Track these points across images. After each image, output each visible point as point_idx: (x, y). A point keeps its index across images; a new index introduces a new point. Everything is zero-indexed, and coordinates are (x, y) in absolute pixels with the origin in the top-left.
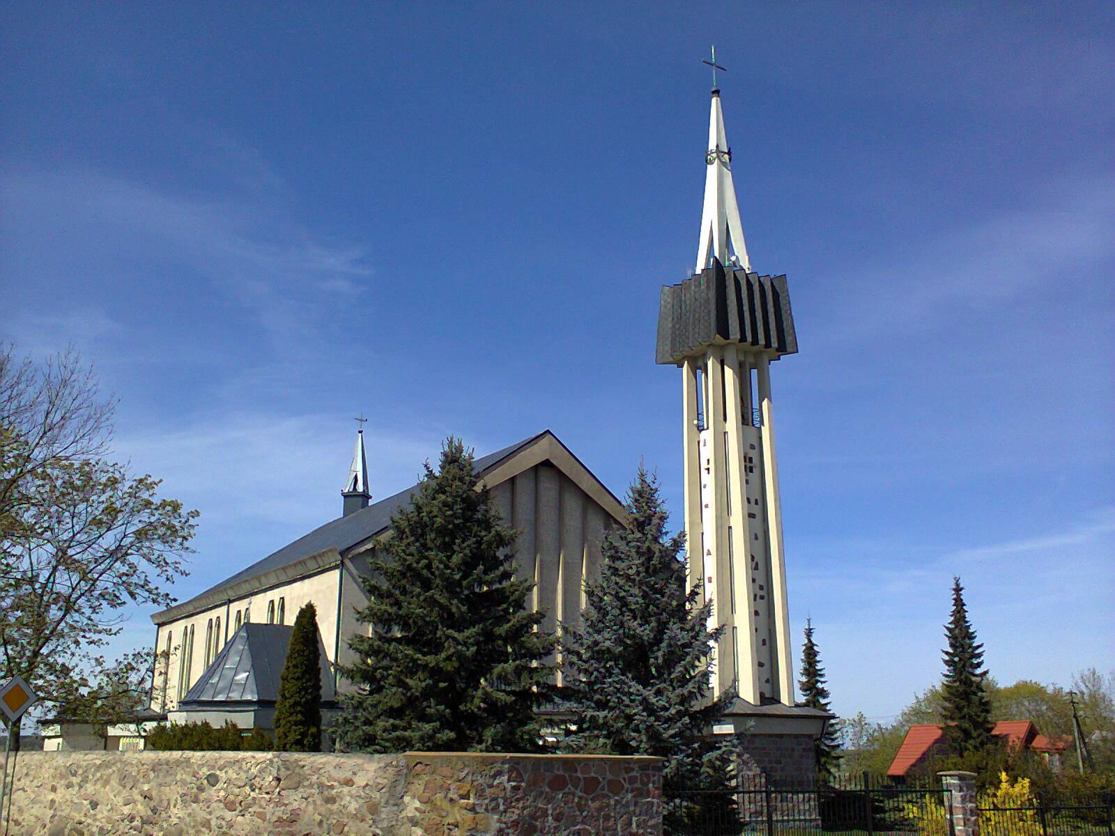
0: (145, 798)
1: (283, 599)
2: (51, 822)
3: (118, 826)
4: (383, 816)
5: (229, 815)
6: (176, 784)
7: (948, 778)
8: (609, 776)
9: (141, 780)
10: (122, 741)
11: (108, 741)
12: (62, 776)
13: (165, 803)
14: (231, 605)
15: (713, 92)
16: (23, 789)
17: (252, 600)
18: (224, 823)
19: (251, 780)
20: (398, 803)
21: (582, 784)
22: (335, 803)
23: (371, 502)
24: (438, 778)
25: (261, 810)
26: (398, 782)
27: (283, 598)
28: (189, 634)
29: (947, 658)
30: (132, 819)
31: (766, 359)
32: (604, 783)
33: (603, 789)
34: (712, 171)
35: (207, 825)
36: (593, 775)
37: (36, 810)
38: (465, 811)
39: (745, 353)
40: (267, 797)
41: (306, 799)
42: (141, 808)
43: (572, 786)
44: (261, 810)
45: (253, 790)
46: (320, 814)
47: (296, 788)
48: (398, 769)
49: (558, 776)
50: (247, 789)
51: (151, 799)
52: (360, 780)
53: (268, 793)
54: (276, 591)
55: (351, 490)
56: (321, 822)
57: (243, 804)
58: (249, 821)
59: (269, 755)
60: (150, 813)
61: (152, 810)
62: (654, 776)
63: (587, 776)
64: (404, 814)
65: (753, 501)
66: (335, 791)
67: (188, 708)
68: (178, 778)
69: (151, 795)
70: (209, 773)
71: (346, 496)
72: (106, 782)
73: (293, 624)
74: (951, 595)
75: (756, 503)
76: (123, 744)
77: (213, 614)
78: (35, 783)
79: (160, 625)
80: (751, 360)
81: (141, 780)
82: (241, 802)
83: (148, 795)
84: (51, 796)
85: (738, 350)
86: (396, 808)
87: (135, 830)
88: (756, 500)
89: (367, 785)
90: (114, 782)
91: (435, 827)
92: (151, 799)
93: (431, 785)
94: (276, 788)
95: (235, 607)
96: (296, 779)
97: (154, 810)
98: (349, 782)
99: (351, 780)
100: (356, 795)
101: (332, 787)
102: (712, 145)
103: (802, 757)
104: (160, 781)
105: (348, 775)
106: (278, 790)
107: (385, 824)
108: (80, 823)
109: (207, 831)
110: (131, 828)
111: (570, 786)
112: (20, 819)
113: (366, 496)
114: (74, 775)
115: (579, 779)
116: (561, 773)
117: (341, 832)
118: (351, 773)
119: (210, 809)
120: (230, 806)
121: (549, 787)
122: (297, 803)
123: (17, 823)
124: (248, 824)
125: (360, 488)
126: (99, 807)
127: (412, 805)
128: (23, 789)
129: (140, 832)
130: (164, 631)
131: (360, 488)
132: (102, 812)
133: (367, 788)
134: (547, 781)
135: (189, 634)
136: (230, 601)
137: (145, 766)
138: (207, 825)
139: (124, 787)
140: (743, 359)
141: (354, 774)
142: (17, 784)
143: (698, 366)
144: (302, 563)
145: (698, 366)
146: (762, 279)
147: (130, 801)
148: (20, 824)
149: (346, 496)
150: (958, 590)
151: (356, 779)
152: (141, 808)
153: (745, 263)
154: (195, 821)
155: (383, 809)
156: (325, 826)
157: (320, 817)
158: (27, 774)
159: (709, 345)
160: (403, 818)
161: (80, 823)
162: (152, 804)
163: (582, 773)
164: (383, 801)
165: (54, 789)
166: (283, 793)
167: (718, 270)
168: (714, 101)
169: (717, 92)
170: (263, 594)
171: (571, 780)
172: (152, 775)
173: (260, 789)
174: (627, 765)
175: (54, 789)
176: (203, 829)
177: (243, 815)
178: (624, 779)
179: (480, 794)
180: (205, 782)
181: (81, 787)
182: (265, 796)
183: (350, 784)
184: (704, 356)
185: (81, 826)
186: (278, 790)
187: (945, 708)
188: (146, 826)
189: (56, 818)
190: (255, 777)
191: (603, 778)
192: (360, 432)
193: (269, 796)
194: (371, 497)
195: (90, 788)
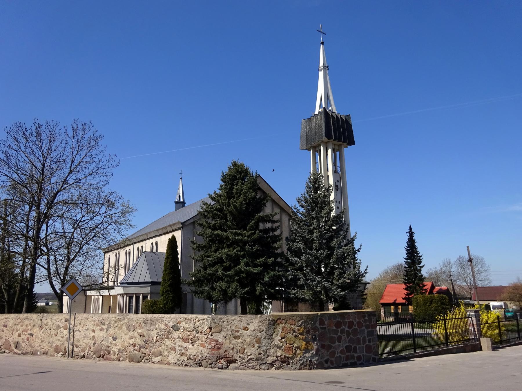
0: (141, 336)
1: (157, 242)
2: (93, 346)
3: (128, 349)
4: (263, 344)
5: (185, 345)
6: (156, 329)
7: (470, 312)
8: (357, 320)
9: (138, 328)
10: (92, 297)
11: (87, 297)
12: (97, 325)
13: (151, 338)
14: (135, 245)
15: (321, 43)
16: (79, 331)
17: (147, 243)
18: (182, 349)
19: (196, 328)
20: (270, 337)
21: (347, 324)
22: (239, 339)
23: (186, 205)
24: (289, 325)
25: (202, 343)
26: (270, 328)
27: (157, 242)
28: (118, 257)
29: (406, 261)
30: (134, 346)
31: (343, 147)
32: (355, 323)
33: (355, 326)
34: (321, 74)
35: (174, 349)
36: (351, 320)
37: (87, 341)
38: (301, 341)
39: (335, 145)
40: (206, 337)
41: (225, 337)
42: (139, 341)
43: (344, 326)
44: (202, 343)
45: (198, 333)
46: (232, 344)
47: (220, 332)
48: (270, 322)
49: (338, 321)
50: (194, 332)
51: (144, 336)
52: (251, 327)
53: (205, 335)
54: (154, 239)
55: (178, 200)
56: (233, 348)
57: (192, 339)
58: (196, 348)
59: (205, 316)
60: (143, 343)
61: (145, 342)
62: (373, 318)
63: (349, 321)
64: (273, 343)
65: (338, 202)
66: (239, 333)
67: (123, 285)
68: (157, 326)
69: (144, 335)
70: (173, 324)
71: (176, 203)
72: (120, 328)
73: (165, 252)
74: (406, 237)
75: (339, 203)
76: (93, 298)
77: (127, 249)
78: (85, 328)
79: (105, 253)
80: (337, 148)
81: (138, 328)
82: (191, 339)
83: (142, 335)
84: (93, 334)
85: (332, 144)
86: (269, 340)
87: (136, 351)
88: (339, 202)
89: (255, 330)
90: (125, 328)
91: (288, 349)
92: (144, 336)
93: (285, 329)
94: (210, 332)
95: (136, 245)
96: (220, 328)
97: (145, 342)
98: (245, 329)
99: (247, 327)
100: (249, 335)
101: (238, 331)
102: (321, 64)
103: (357, 298)
104: (148, 328)
105: (245, 325)
106: (211, 333)
107: (264, 348)
108: (108, 347)
109: (174, 352)
110: (134, 350)
111: (343, 326)
112: (78, 344)
113: (183, 203)
114: (104, 324)
115: (346, 322)
116: (339, 320)
117: (243, 353)
118: (246, 324)
119: (175, 342)
120: (185, 340)
121: (335, 327)
122: (221, 339)
123: (77, 346)
124: (195, 349)
125: (182, 200)
126: (117, 340)
127: (277, 339)
128: (79, 331)
129: (139, 352)
130: (107, 255)
131: (182, 200)
132: (119, 341)
133: (255, 331)
134: (334, 324)
135: (118, 257)
136: (135, 243)
137: (139, 321)
138: (174, 349)
139: (129, 330)
140: (334, 147)
141: (248, 324)
142: (76, 329)
143: (317, 150)
144: (165, 228)
145: (317, 150)
146: (341, 116)
147: (133, 337)
148: (78, 347)
149: (176, 203)
150: (411, 233)
151: (249, 327)
152: (139, 341)
153: (335, 111)
154: (167, 347)
155: (263, 341)
156: (235, 350)
157: (233, 346)
158: (80, 324)
159: (321, 142)
160: (273, 345)
161: (108, 347)
162: (144, 339)
163: (347, 319)
164: (263, 337)
165: (94, 331)
166: (214, 334)
167: (326, 114)
168: (322, 46)
169: (323, 43)
170: (148, 240)
171: (343, 323)
172: (143, 325)
173: (201, 332)
174: (363, 314)
175: (94, 331)
176: (172, 351)
177: (193, 345)
178: (363, 321)
179: (308, 332)
180: (172, 329)
181: (107, 330)
182: (205, 336)
183: (247, 329)
184: (319, 146)
185: (109, 348)
186: (211, 333)
187: (405, 279)
188: (142, 349)
189: (96, 344)
190: (198, 327)
191: (355, 321)
192: (181, 178)
193: (206, 336)
194: (185, 203)
195: (111, 331)
